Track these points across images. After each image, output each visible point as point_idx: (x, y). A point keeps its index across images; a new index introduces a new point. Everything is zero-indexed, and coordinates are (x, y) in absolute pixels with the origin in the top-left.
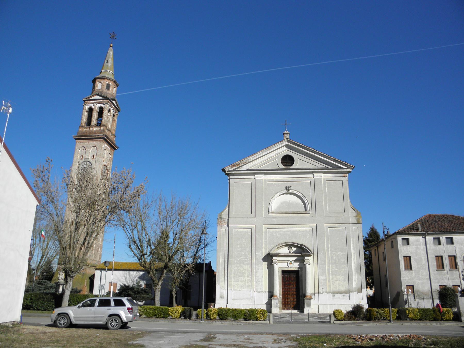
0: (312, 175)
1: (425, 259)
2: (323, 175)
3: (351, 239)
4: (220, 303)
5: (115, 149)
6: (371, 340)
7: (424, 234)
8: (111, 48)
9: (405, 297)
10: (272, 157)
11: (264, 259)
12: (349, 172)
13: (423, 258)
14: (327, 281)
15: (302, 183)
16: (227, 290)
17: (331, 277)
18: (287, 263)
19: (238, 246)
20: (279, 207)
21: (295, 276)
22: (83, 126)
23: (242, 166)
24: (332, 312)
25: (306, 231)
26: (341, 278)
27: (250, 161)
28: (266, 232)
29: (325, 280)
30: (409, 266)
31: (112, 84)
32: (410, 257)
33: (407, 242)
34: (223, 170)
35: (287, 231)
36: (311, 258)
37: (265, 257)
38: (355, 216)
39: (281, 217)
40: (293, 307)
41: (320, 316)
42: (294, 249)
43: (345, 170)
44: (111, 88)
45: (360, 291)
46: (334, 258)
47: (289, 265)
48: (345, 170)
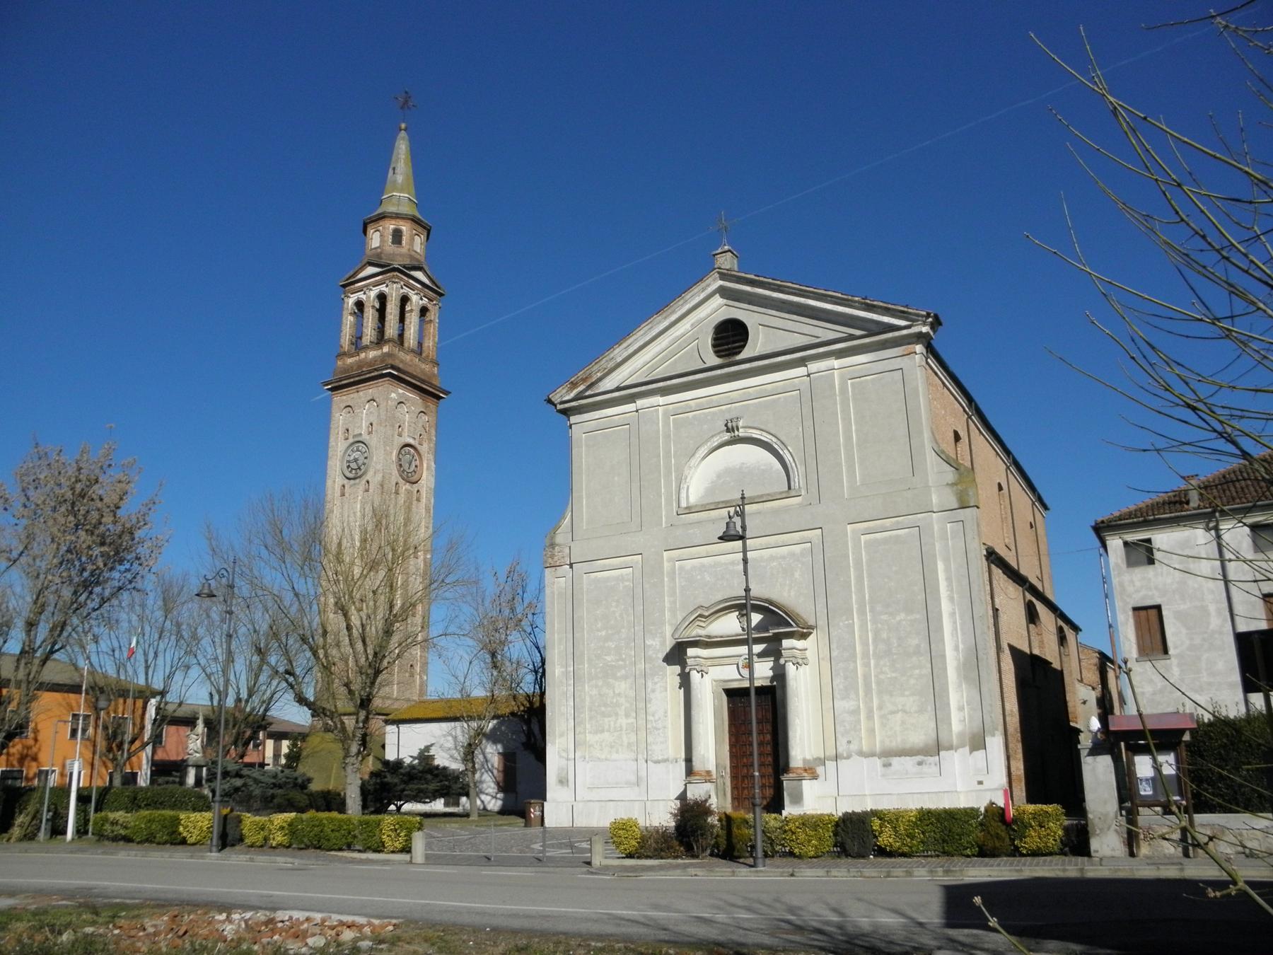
2: (836, 363)
5: (439, 398)
7: (1209, 517)
8: (403, 134)
13: (1212, 608)
14: (863, 716)
15: (774, 401)
19: (599, 625)
20: (710, 491)
22: (344, 354)
23: (600, 379)
25: (792, 554)
26: (911, 702)
27: (619, 359)
29: (856, 712)
31: (405, 227)
33: (1143, 554)
34: (549, 401)
36: (808, 643)
42: (756, 618)
43: (905, 332)
45: (978, 743)
48: (905, 332)
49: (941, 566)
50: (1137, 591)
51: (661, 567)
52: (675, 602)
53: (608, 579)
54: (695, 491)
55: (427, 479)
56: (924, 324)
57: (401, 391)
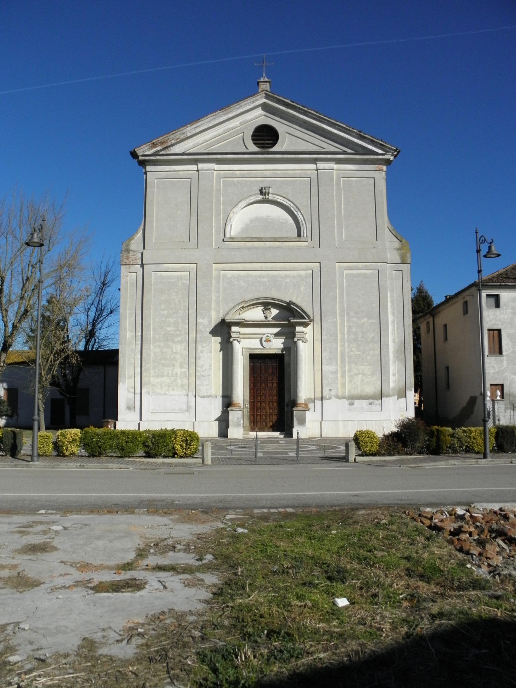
0: (313, 166)
2: (336, 166)
3: (389, 295)
4: (126, 421)
6: (434, 496)
9: (489, 406)
10: (233, 128)
11: (214, 332)
12: (388, 162)
14: (339, 375)
16: (141, 394)
17: (347, 367)
18: (261, 340)
19: (163, 307)
20: (245, 229)
21: (276, 364)
23: (173, 145)
24: (352, 435)
25: (300, 276)
26: (367, 369)
27: (189, 135)
28: (218, 278)
29: (336, 372)
30: (498, 349)
32: (499, 331)
33: (497, 303)
34: (134, 155)
35: (260, 276)
36: (308, 330)
37: (216, 326)
38: (398, 249)
39: (249, 249)
40: (271, 427)
41: (323, 444)
42: (274, 312)
43: (381, 157)
45: (402, 394)
47: (264, 343)
48: (381, 157)
50: (490, 321)
51: (211, 273)
52: (219, 297)
54: (235, 228)
56: (392, 155)
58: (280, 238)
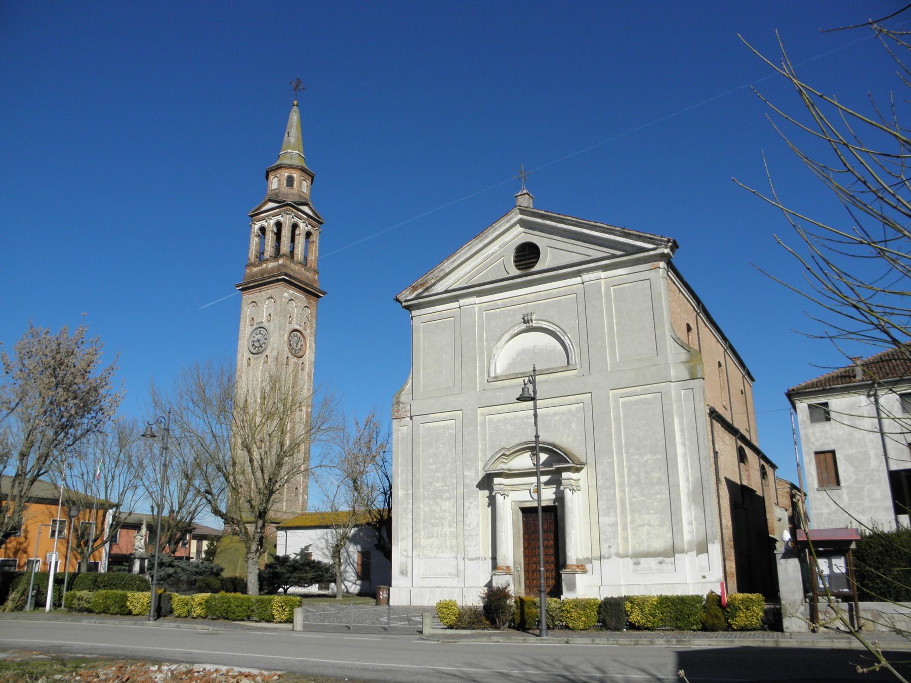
1: (877, 455)
2: (603, 274)
5: (318, 297)
7: (870, 387)
8: (295, 108)
12: (663, 257)
13: (872, 453)
14: (619, 528)
17: (629, 518)
20: (512, 365)
22: (251, 265)
23: (433, 285)
25: (570, 411)
26: (654, 519)
27: (447, 271)
28: (484, 423)
29: (615, 525)
31: (296, 175)
32: (833, 452)
33: (822, 413)
34: (397, 300)
43: (652, 253)
44: (295, 184)
45: (702, 548)
46: (636, 470)
48: (652, 253)
49: (676, 421)
50: (817, 440)
52: (485, 445)
53: (437, 428)
54: (500, 365)
55: (309, 355)
56: (666, 247)
57: (291, 292)
58: (546, 370)
